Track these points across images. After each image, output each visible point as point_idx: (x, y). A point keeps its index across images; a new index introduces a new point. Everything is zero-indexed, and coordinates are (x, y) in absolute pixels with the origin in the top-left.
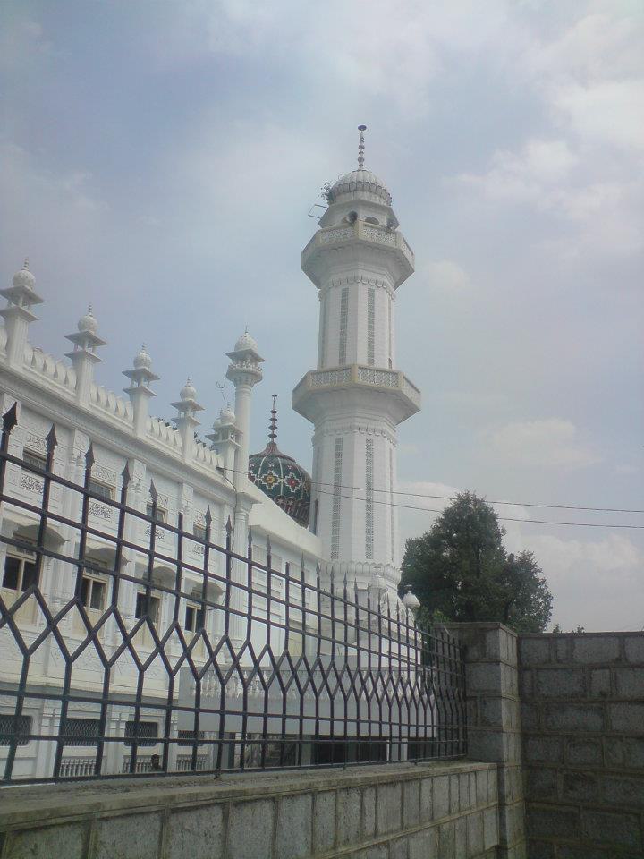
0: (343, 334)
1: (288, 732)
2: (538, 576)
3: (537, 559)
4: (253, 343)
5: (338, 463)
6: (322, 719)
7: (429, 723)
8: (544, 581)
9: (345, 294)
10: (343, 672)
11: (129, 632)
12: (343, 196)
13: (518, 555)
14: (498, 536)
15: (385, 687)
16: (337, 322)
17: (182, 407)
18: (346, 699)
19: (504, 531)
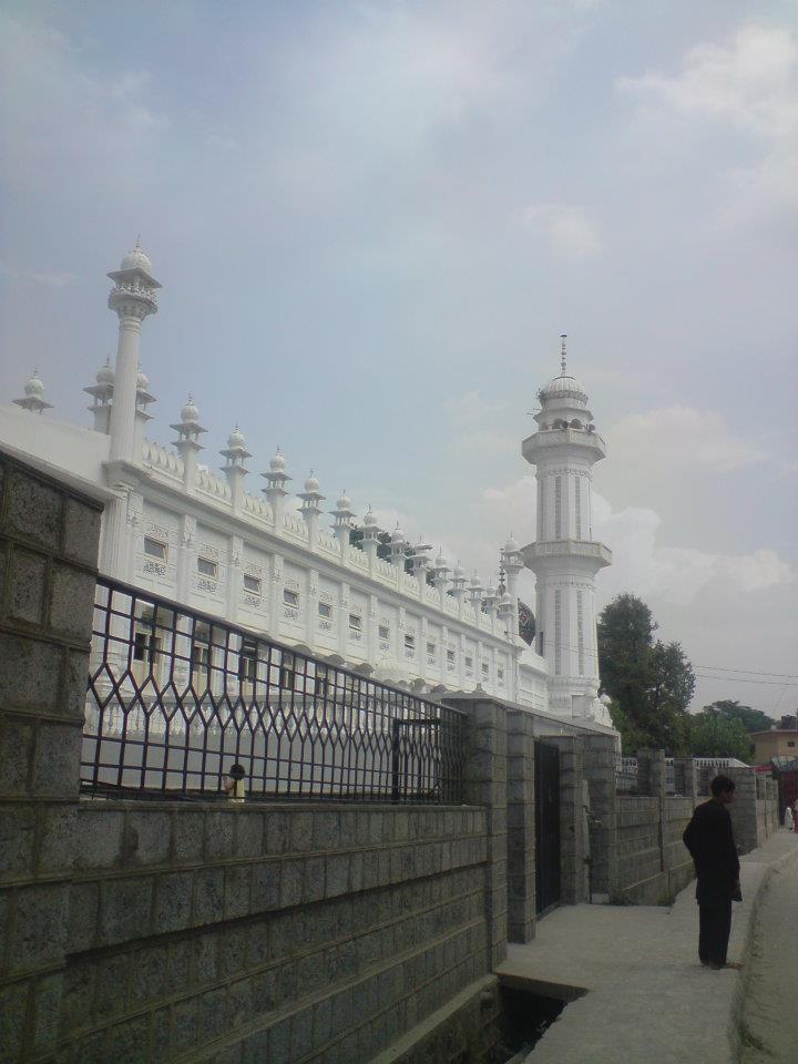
0: (558, 513)
1: (254, 789)
2: (685, 662)
3: (685, 648)
4: (145, 260)
5: (558, 607)
6: (91, 764)
7: (426, 779)
8: (689, 665)
9: (558, 480)
10: (237, 704)
11: (117, 681)
12: (553, 401)
13: (666, 644)
14: (650, 629)
15: (286, 721)
16: (551, 501)
17: (272, 477)
18: (313, 744)
19: (656, 626)
